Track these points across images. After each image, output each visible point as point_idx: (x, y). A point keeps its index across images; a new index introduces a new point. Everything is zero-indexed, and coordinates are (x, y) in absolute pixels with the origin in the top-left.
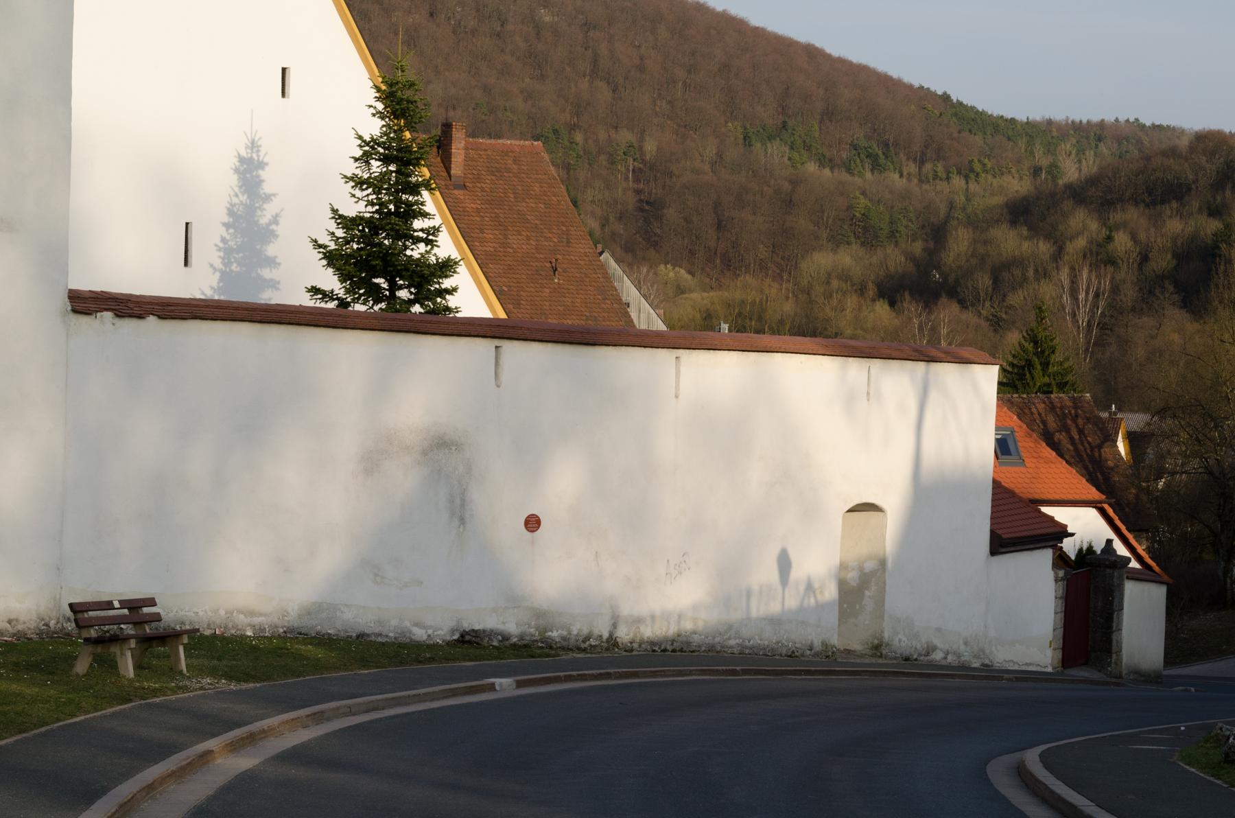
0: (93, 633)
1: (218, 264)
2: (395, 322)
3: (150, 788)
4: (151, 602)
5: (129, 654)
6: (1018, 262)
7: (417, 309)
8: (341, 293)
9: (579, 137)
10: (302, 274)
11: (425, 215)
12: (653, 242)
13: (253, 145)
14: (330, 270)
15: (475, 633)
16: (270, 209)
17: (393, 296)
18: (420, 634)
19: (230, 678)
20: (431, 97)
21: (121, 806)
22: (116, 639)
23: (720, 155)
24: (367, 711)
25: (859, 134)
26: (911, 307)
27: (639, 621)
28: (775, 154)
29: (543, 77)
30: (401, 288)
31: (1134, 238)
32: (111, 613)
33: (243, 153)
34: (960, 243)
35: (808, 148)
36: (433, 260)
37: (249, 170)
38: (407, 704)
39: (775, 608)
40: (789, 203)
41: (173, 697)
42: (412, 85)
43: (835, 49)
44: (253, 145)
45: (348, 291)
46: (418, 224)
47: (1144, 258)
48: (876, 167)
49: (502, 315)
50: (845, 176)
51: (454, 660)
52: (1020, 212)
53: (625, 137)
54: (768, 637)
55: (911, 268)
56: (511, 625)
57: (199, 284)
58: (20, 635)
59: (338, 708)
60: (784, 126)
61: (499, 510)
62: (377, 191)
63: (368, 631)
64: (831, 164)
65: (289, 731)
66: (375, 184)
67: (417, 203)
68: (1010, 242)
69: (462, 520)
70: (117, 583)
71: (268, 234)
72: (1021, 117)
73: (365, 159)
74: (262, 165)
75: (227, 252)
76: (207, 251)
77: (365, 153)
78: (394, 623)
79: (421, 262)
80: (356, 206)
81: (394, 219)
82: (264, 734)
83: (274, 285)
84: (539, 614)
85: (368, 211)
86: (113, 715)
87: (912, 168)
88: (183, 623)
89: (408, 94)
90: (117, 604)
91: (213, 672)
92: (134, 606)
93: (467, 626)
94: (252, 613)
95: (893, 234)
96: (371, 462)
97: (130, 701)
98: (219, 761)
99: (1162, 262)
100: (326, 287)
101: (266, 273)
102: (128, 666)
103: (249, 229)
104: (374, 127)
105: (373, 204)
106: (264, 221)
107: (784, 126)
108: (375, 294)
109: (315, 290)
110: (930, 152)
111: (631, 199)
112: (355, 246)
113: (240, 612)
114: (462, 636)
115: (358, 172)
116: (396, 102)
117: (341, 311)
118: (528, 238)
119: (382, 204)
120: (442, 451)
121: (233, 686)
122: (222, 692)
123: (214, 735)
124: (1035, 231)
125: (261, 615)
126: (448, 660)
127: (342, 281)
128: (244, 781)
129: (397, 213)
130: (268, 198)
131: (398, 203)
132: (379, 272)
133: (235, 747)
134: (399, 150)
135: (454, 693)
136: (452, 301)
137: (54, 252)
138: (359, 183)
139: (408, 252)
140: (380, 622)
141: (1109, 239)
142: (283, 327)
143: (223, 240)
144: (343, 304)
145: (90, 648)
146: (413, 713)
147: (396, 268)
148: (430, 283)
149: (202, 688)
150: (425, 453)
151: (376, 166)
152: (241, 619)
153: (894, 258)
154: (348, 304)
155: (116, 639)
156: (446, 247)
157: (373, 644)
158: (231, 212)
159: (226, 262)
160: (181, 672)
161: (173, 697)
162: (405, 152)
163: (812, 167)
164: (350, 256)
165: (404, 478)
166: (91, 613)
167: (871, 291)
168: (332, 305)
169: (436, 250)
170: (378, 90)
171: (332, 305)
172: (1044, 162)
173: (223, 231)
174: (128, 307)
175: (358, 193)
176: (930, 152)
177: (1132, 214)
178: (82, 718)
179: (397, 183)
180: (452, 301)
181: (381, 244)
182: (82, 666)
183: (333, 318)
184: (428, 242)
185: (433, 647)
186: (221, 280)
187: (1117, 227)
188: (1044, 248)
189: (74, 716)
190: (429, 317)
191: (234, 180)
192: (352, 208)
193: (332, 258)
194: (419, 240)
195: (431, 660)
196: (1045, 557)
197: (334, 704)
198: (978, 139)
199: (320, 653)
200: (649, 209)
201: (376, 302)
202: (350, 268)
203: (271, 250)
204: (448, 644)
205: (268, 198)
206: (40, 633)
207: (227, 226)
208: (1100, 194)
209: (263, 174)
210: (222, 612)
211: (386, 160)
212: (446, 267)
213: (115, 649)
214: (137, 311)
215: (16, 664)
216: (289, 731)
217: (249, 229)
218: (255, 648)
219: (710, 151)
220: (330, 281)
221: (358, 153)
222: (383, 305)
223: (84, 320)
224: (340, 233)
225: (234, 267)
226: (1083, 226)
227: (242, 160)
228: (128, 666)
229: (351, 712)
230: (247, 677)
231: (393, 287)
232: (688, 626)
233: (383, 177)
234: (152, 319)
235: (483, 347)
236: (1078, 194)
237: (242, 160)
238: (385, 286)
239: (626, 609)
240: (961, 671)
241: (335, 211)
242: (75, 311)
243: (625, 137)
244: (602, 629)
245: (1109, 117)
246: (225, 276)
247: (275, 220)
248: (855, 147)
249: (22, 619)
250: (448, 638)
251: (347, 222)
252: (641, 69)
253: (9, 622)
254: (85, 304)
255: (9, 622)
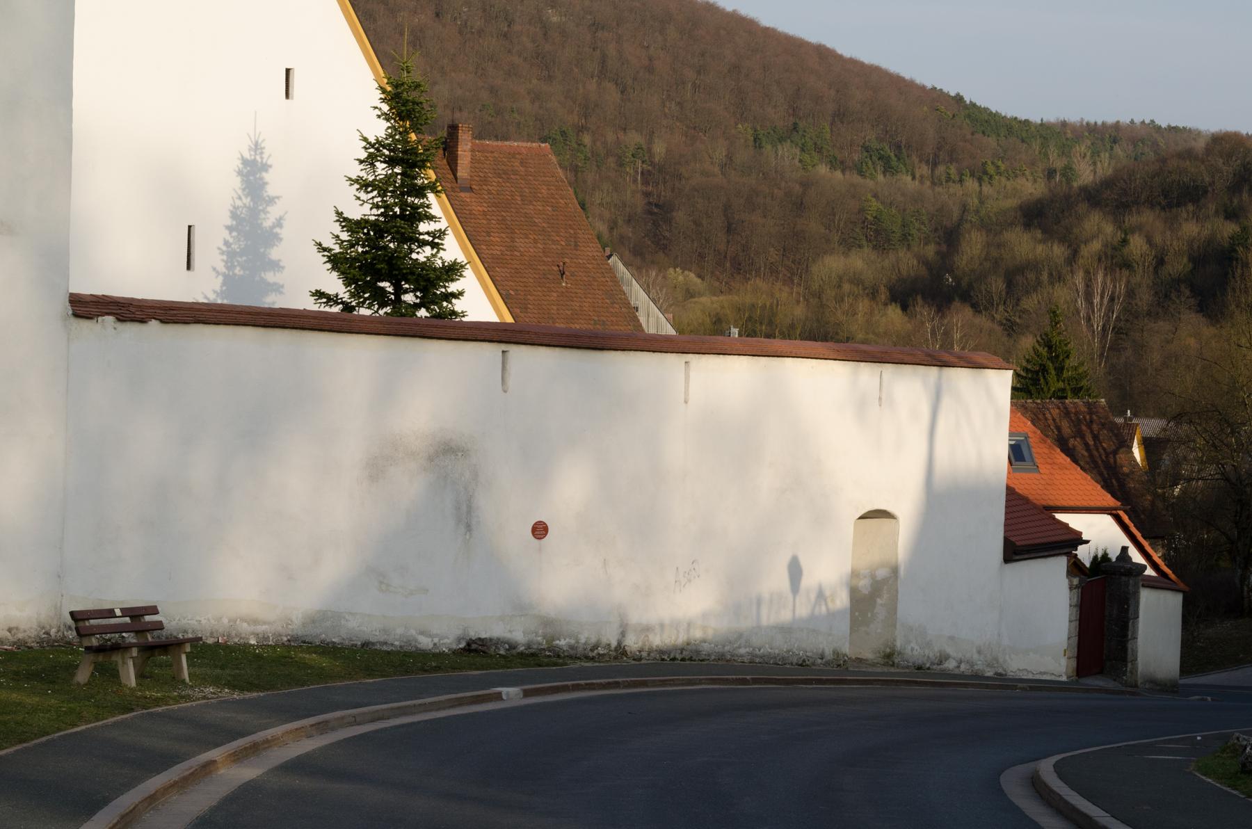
0: (94, 642)
1: (221, 267)
2: (401, 326)
3: (152, 799)
4: (153, 610)
5: (131, 663)
6: (1032, 266)
7: (423, 313)
8: (346, 297)
9: (587, 139)
10: (306, 278)
11: (431, 218)
12: (662, 245)
13: (257, 147)
14: (335, 274)
15: (482, 642)
16: (274, 212)
17: (398, 300)
18: (425, 643)
19: (233, 687)
20: (437, 98)
21: (123, 817)
22: (118, 648)
23: (730, 157)
24: (373, 721)
25: (871, 136)
26: (924, 311)
27: (647, 629)
28: (785, 156)
29: (550, 78)
30: (406, 291)
31: (1149, 241)
32: (113, 621)
33: (247, 155)
34: (973, 247)
35: (819, 150)
36: (439, 263)
37: (253, 173)
38: (413, 714)
39: (785, 616)
40: (799, 206)
41: (176, 707)
42: (418, 86)
43: (846, 49)
44: (257, 147)
45: (352, 295)
46: (423, 227)
47: (1160, 262)
48: (888, 169)
49: (509, 319)
50: (857, 179)
51: (461, 669)
52: (1034, 215)
53: (634, 138)
54: (779, 646)
55: (923, 271)
56: (519, 633)
57: (201, 288)
58: (20, 644)
59: (343, 718)
60: (795, 128)
61: (506, 517)
62: (382, 193)
63: (373, 639)
64: (843, 166)
65: (293, 741)
66: (380, 187)
67: (422, 205)
68: (1024, 245)
69: (469, 527)
70: (119, 591)
71: (271, 237)
72: (1035, 118)
73: (370, 161)
74: (265, 167)
75: (230, 256)
76: (209, 255)
77: (370, 155)
78: (400, 631)
79: (427, 266)
80: (361, 208)
81: (399, 222)
82: (268, 744)
83: (277, 288)
84: (547, 622)
85: (373, 214)
86: (115, 724)
87: (925, 170)
88: (185, 632)
89: (413, 95)
90: (118, 613)
91: (216, 681)
92: (136, 614)
93: (473, 634)
94: (255, 622)
95: (905, 237)
96: (377, 468)
97: (132, 710)
98: (222, 771)
99: (1178, 266)
100: (331, 291)
101: (270, 277)
102: (129, 675)
103: (253, 232)
104: (379, 129)
105: (378, 207)
106: (267, 224)
107: (795, 128)
108: (380, 298)
109: (319, 294)
110: (943, 154)
111: (640, 202)
112: (360, 250)
113: (243, 620)
114: (469, 644)
115: (363, 174)
116: (401, 103)
117: (346, 315)
118: (535, 241)
119: (387, 207)
120: (448, 457)
121: (236, 696)
122: (225, 701)
123: (217, 745)
124: (1049, 234)
125: (265, 623)
126: (454, 669)
127: (347, 285)
128: (248, 791)
129: (402, 216)
130: (272, 201)
131: (403, 206)
132: (384, 276)
133: (238, 757)
134: (405, 152)
135: (460, 702)
136: (458, 305)
137: (55, 256)
138: (364, 185)
139: (414, 256)
140: (385, 631)
141: (1125, 242)
142: (287, 332)
143: (226, 243)
144: (348, 308)
145: (91, 657)
146: (419, 722)
147: (402, 271)
148: (436, 286)
149: (204, 698)
150: (431, 459)
151: (381, 168)
152: (244, 628)
153: (906, 262)
154: (353, 308)
155: (118, 648)
156: (453, 250)
157: (378, 653)
158: (234, 215)
159: (229, 265)
160: (183, 681)
161: (176, 707)
162: (410, 154)
163: (823, 169)
164: (355, 259)
165: (409, 485)
166: (92, 622)
167: (883, 295)
168: (336, 309)
169: (442, 253)
170: (384, 91)
171: (336, 309)
172: (1059, 164)
173: (226, 234)
174: (129, 311)
175: (363, 196)
176: (943, 154)
177: (1147, 217)
178: (83, 727)
179: (402, 185)
180: (458, 305)
181: (386, 248)
182: (83, 675)
183: (338, 323)
184: (434, 245)
185: (439, 656)
186: (224, 284)
187: (1132, 230)
188: (1058, 251)
189: (75, 725)
190: (435, 321)
191: (237, 182)
192: (357, 211)
193: (336, 262)
194: (425, 243)
195: (437, 669)
196: (1059, 565)
197: (338, 714)
198: (992, 141)
199: (325, 662)
200: (658, 212)
201: (382, 306)
202: (355, 272)
203: (274, 253)
204: (455, 652)
205: (272, 201)
206: (41, 642)
207: (230, 229)
208: (1115, 197)
209: (267, 176)
210: (225, 621)
211: (391, 162)
212: (452, 271)
213: (116, 658)
214: (139, 315)
215: (17, 673)
216: (293, 741)
217: (253, 232)
218: (259, 657)
219: (720, 153)
220: (335, 285)
221: (363, 155)
222: (388, 309)
223: (85, 325)
224: (345, 236)
225: (238, 271)
226: (1098, 229)
227: (245, 162)
228: (129, 675)
229: (356, 722)
230: (251, 687)
231: (399, 291)
232: (697, 634)
233: (389, 179)
234: (154, 323)
235: (490, 352)
236: (1093, 197)
237: (245, 162)
238: (390, 290)
239: (635, 618)
240: (975, 680)
241: (339, 214)
242: (76, 315)
243: (634, 138)
244: (610, 637)
245: (1125, 119)
246: (228, 280)
247: (279, 223)
248: (867, 149)
249: (22, 627)
250: (454, 647)
251: (351, 225)
252: (650, 69)
253: (10, 630)
254: (86, 308)
255: (10, 630)
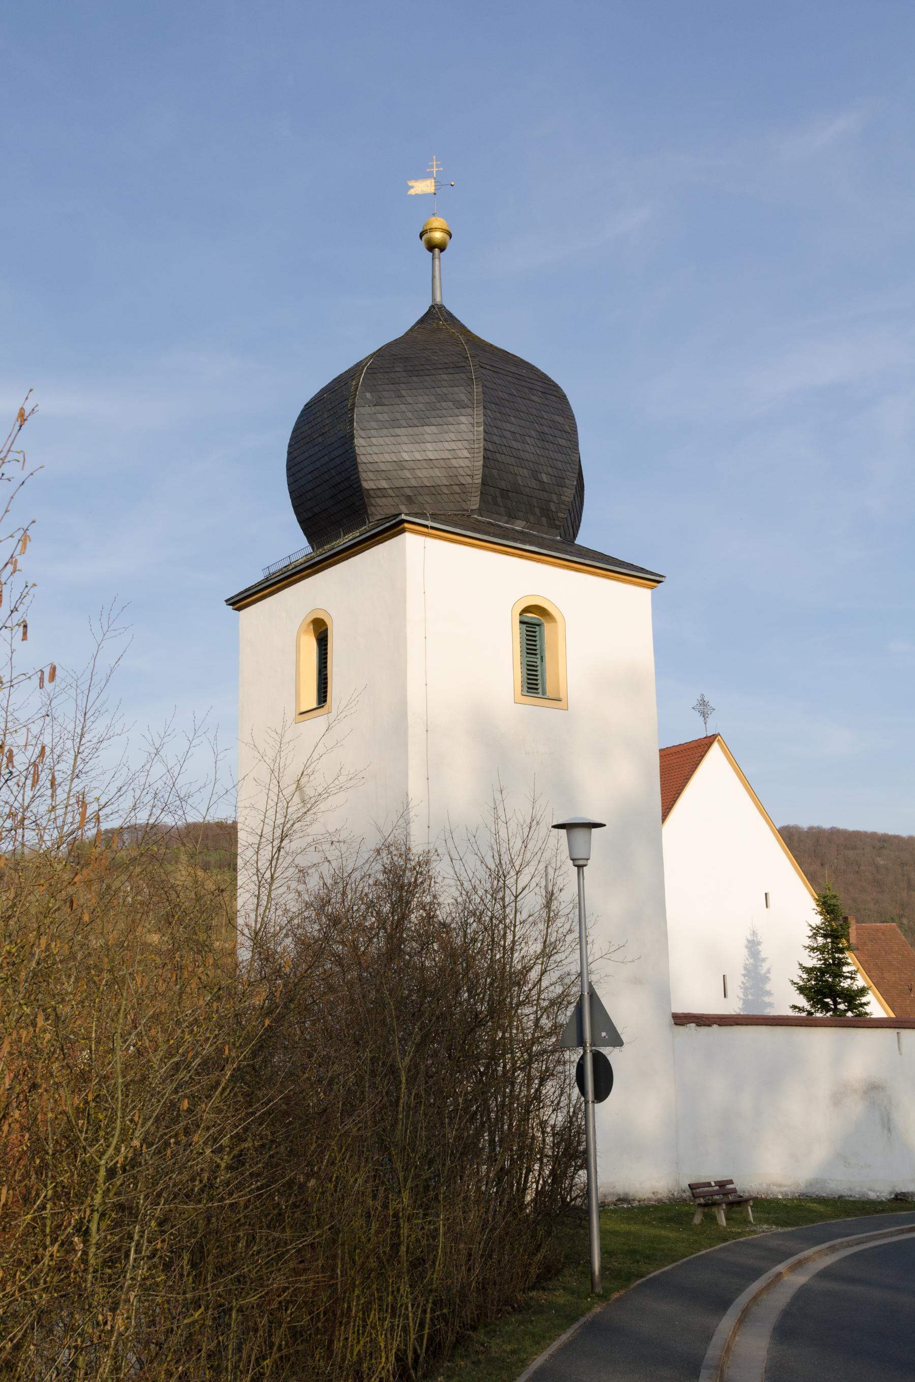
0: (702, 1201)
1: (742, 996)
2: (839, 1021)
3: (755, 1298)
4: (731, 1182)
5: (722, 1213)
7: (849, 1014)
8: (809, 1008)
10: (787, 999)
11: (848, 964)
13: (754, 933)
14: (802, 996)
15: (903, 1194)
16: (765, 967)
17: (836, 1008)
18: (872, 1195)
19: (777, 1225)
20: (844, 903)
21: (743, 1312)
22: (715, 1204)
24: (858, 1244)
29: (882, 892)
30: (840, 1003)
32: (710, 1189)
33: (749, 938)
36: (855, 988)
37: (753, 946)
38: (878, 1239)
41: (750, 1238)
42: (835, 897)
44: (754, 933)
45: (812, 1006)
46: (845, 969)
49: (893, 1015)
51: (896, 1210)
57: (733, 1007)
58: (659, 1201)
59: (842, 1243)
62: (822, 953)
63: (844, 1194)
65: (820, 1259)
66: (821, 949)
67: (844, 958)
69: (889, 1130)
70: (711, 1171)
71: (765, 979)
73: (814, 936)
74: (759, 943)
75: (746, 989)
76: (735, 989)
77: (814, 934)
78: (858, 1189)
79: (848, 989)
80: (813, 961)
81: (833, 967)
82: (807, 1259)
83: (771, 1005)
85: (819, 964)
86: (721, 1249)
88: (744, 1192)
89: (833, 901)
90: (713, 1184)
91: (767, 1221)
92: (722, 1184)
93: (898, 1190)
94: (780, 1186)
96: (837, 1098)
97: (727, 1240)
98: (786, 1278)
100: (800, 1005)
101: (766, 999)
102: (722, 1220)
103: (756, 977)
104: (817, 920)
105: (820, 960)
106: (763, 972)
108: (826, 1008)
109: (794, 1007)
112: (813, 983)
113: (774, 1185)
114: (896, 1196)
115: (811, 943)
116: (827, 906)
117: (810, 1017)
118: (895, 974)
119: (826, 960)
120: (874, 1091)
121: (780, 1230)
122: (775, 1234)
123: (780, 1262)
125: (785, 1186)
126: (892, 1211)
127: (809, 1001)
128: (803, 1293)
129: (834, 964)
130: (764, 960)
131: (834, 958)
132: (826, 995)
133: (793, 1268)
134: (832, 931)
135: (902, 1232)
136: (868, 1009)
137: (663, 993)
138: (813, 949)
139: (842, 984)
140: (850, 1189)
142: (783, 1027)
143: (743, 983)
144: (810, 1013)
145: (700, 1210)
146: (884, 1245)
147: (834, 992)
148: (856, 1000)
149: (763, 1232)
150: (865, 1093)
151: (821, 941)
152: (775, 1189)
154: (812, 1014)
155: (715, 1204)
156: (860, 982)
157: (849, 1201)
158: (745, 969)
159: (745, 994)
160: (750, 1222)
161: (750, 1238)
162: (834, 933)
164: (811, 988)
165: (856, 1107)
166: (701, 1189)
168: (804, 1014)
169: (856, 982)
170: (818, 901)
171: (804, 1014)
173: (742, 978)
174: (703, 1021)
175: (812, 954)
178: (704, 1252)
179: (832, 948)
180: (868, 1009)
181: (827, 981)
182: (697, 1219)
183: (808, 1022)
184: (852, 978)
185: (881, 1202)
186: (744, 1004)
189: (700, 1251)
190: (858, 1018)
193: (801, 990)
194: (847, 977)
195: (883, 1211)
197: (839, 1241)
199: (821, 1208)
201: (827, 1012)
202: (812, 994)
203: (768, 987)
204: (889, 1200)
205: (764, 960)
206: (670, 1199)
207: (744, 975)
209: (760, 948)
210: (765, 1186)
211: (825, 936)
212: (862, 991)
213: (715, 1209)
214: (707, 1022)
215: (661, 1218)
216: (820, 1259)
217: (756, 977)
218: (785, 1206)
220: (802, 1002)
221: (811, 934)
222: (831, 1013)
223: (681, 1028)
224: (805, 976)
225: (750, 997)
227: (749, 941)
228: (722, 1220)
229: (849, 1245)
230: (785, 1224)
231: (836, 1003)
233: (825, 946)
234: (715, 1026)
235: (890, 1033)
237: (749, 941)
238: (831, 1003)
241: (801, 965)
242: (676, 1024)
246: (746, 1002)
247: (769, 971)
249: (660, 1191)
250: (889, 1197)
251: (809, 971)
253: (653, 1193)
254: (681, 1020)
255: (653, 1193)
